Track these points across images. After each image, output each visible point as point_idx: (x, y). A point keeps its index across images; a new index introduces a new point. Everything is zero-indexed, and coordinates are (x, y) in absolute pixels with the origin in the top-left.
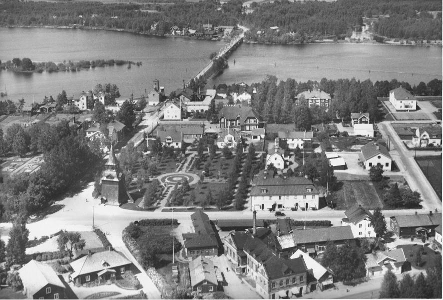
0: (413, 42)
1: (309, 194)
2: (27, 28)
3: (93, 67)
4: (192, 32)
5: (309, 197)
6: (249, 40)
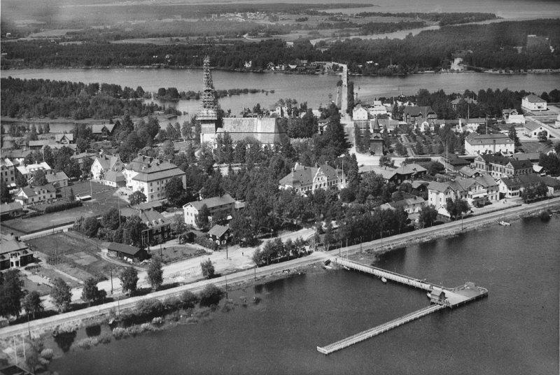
0: (511, 71)
1: (508, 143)
2: (105, 69)
3: (230, 95)
4: (293, 67)
5: (508, 145)
6: (354, 72)
